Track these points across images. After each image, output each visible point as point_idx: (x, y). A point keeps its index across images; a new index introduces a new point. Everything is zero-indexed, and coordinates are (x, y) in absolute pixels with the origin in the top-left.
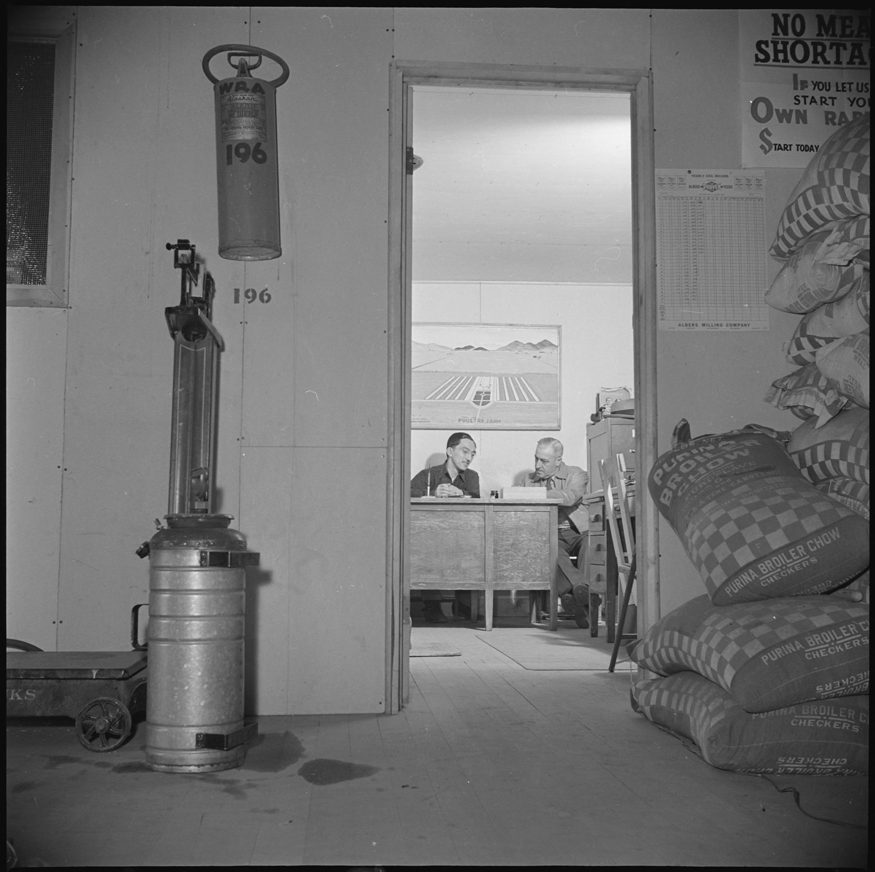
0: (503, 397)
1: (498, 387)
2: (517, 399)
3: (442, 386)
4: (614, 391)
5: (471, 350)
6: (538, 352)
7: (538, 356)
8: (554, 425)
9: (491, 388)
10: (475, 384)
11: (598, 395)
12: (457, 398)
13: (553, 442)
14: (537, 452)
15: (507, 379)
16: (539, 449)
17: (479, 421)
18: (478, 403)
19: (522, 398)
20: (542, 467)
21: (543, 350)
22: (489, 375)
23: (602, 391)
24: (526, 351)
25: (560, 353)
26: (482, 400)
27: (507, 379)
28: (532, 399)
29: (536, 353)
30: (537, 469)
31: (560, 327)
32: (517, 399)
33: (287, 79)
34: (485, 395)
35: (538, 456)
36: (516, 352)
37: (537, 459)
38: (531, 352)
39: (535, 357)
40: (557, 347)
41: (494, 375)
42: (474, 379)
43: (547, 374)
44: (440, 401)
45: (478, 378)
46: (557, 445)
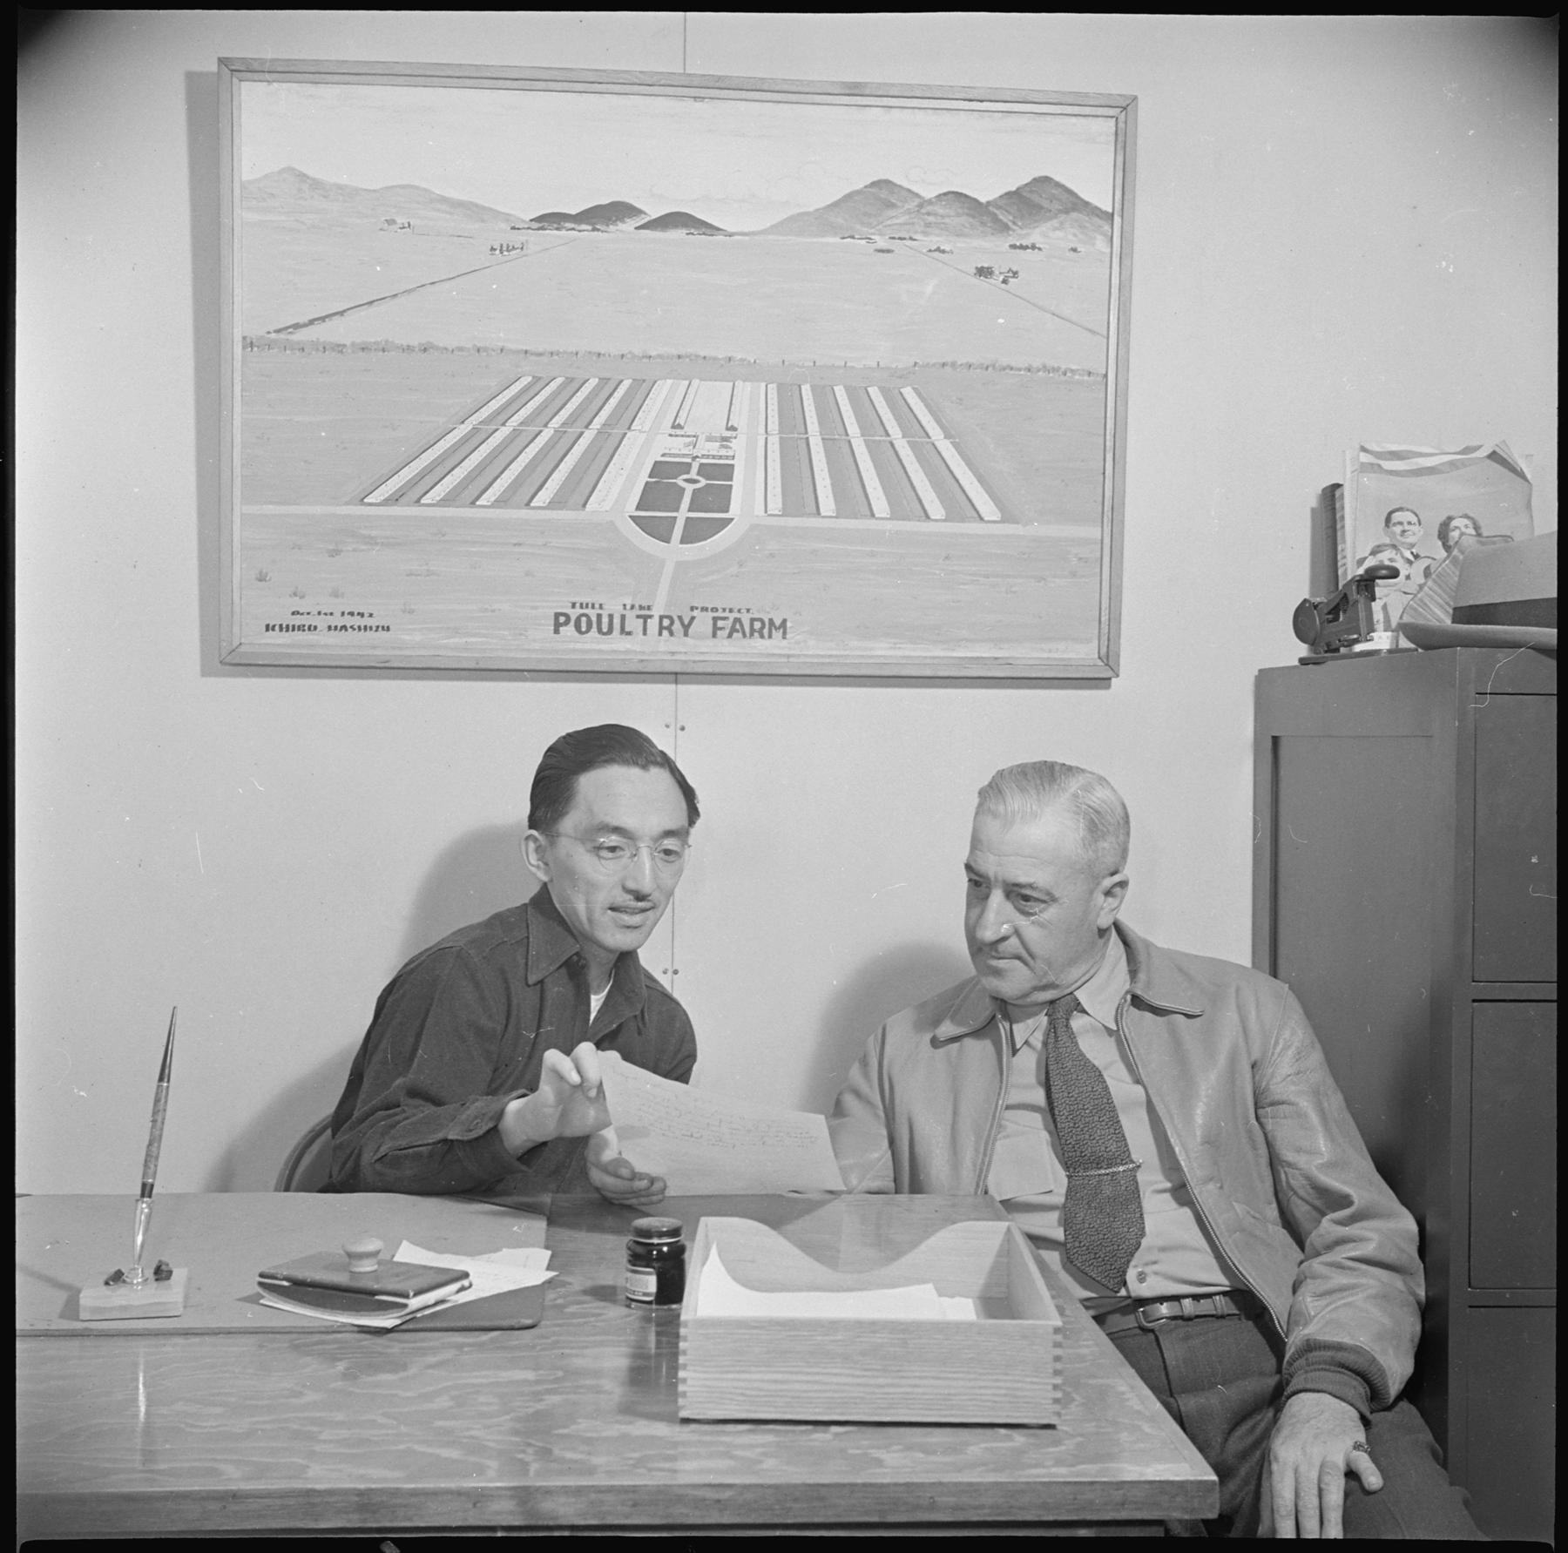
0: (799, 497)
1: (774, 442)
2: (880, 505)
3: (463, 430)
4: (1431, 471)
5: (629, 225)
6: (1003, 243)
7: (1000, 266)
8: (1082, 653)
9: (738, 446)
10: (644, 421)
11: (1331, 495)
12: (543, 497)
13: (1074, 784)
14: (976, 843)
15: (824, 396)
16: (992, 827)
17: (666, 626)
18: (659, 532)
19: (905, 504)
20: (1017, 932)
21: (1035, 237)
22: (724, 369)
23: (1365, 468)
24: (934, 240)
25: (1126, 254)
26: (683, 514)
27: (824, 396)
28: (959, 507)
29: (991, 248)
30: (981, 950)
31: (1125, 108)
32: (880, 505)
33: (672, 213)
34: (703, 482)
35: (989, 865)
36: (882, 242)
37: (979, 884)
38: (961, 243)
39: (984, 272)
40: (1110, 217)
41: (753, 372)
42: (642, 389)
43: (1045, 368)
44: (383, 511)
45: (663, 389)
46: (1100, 795)
